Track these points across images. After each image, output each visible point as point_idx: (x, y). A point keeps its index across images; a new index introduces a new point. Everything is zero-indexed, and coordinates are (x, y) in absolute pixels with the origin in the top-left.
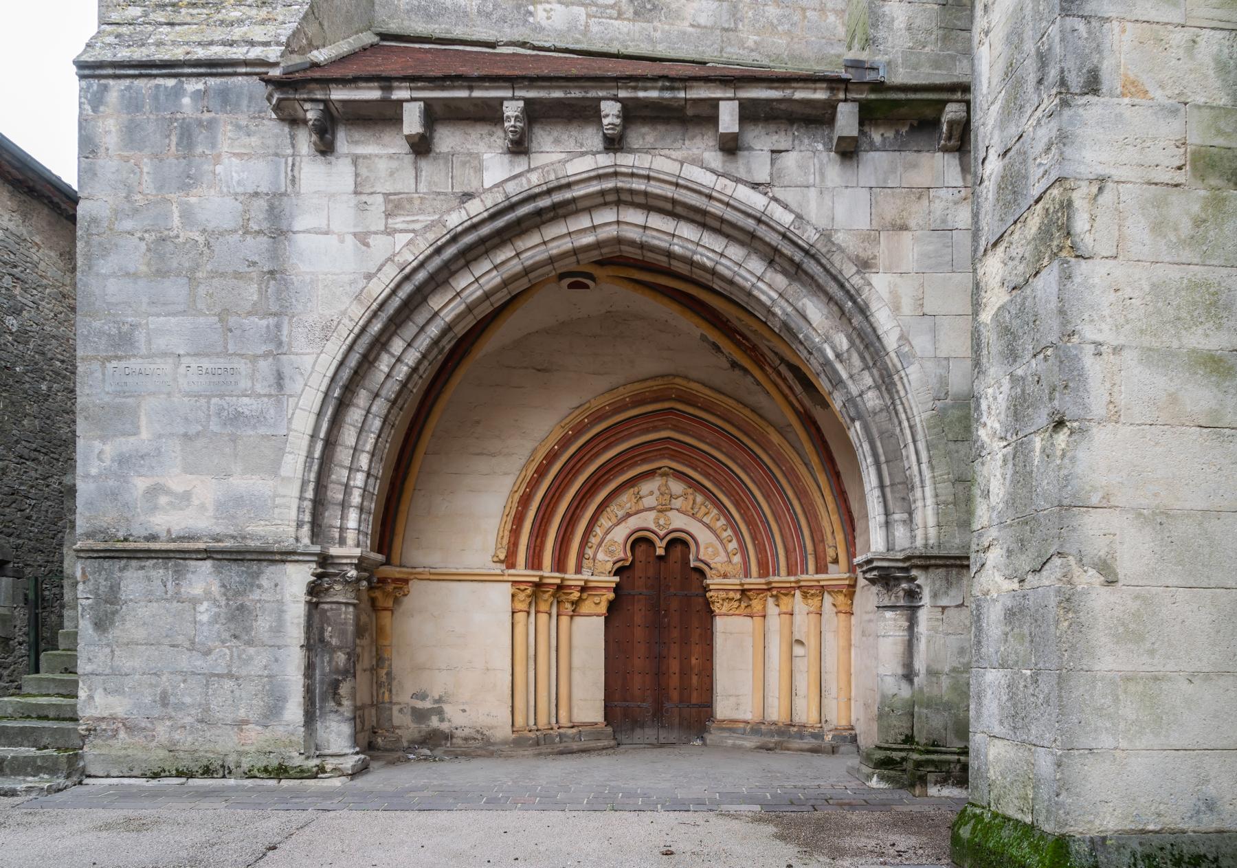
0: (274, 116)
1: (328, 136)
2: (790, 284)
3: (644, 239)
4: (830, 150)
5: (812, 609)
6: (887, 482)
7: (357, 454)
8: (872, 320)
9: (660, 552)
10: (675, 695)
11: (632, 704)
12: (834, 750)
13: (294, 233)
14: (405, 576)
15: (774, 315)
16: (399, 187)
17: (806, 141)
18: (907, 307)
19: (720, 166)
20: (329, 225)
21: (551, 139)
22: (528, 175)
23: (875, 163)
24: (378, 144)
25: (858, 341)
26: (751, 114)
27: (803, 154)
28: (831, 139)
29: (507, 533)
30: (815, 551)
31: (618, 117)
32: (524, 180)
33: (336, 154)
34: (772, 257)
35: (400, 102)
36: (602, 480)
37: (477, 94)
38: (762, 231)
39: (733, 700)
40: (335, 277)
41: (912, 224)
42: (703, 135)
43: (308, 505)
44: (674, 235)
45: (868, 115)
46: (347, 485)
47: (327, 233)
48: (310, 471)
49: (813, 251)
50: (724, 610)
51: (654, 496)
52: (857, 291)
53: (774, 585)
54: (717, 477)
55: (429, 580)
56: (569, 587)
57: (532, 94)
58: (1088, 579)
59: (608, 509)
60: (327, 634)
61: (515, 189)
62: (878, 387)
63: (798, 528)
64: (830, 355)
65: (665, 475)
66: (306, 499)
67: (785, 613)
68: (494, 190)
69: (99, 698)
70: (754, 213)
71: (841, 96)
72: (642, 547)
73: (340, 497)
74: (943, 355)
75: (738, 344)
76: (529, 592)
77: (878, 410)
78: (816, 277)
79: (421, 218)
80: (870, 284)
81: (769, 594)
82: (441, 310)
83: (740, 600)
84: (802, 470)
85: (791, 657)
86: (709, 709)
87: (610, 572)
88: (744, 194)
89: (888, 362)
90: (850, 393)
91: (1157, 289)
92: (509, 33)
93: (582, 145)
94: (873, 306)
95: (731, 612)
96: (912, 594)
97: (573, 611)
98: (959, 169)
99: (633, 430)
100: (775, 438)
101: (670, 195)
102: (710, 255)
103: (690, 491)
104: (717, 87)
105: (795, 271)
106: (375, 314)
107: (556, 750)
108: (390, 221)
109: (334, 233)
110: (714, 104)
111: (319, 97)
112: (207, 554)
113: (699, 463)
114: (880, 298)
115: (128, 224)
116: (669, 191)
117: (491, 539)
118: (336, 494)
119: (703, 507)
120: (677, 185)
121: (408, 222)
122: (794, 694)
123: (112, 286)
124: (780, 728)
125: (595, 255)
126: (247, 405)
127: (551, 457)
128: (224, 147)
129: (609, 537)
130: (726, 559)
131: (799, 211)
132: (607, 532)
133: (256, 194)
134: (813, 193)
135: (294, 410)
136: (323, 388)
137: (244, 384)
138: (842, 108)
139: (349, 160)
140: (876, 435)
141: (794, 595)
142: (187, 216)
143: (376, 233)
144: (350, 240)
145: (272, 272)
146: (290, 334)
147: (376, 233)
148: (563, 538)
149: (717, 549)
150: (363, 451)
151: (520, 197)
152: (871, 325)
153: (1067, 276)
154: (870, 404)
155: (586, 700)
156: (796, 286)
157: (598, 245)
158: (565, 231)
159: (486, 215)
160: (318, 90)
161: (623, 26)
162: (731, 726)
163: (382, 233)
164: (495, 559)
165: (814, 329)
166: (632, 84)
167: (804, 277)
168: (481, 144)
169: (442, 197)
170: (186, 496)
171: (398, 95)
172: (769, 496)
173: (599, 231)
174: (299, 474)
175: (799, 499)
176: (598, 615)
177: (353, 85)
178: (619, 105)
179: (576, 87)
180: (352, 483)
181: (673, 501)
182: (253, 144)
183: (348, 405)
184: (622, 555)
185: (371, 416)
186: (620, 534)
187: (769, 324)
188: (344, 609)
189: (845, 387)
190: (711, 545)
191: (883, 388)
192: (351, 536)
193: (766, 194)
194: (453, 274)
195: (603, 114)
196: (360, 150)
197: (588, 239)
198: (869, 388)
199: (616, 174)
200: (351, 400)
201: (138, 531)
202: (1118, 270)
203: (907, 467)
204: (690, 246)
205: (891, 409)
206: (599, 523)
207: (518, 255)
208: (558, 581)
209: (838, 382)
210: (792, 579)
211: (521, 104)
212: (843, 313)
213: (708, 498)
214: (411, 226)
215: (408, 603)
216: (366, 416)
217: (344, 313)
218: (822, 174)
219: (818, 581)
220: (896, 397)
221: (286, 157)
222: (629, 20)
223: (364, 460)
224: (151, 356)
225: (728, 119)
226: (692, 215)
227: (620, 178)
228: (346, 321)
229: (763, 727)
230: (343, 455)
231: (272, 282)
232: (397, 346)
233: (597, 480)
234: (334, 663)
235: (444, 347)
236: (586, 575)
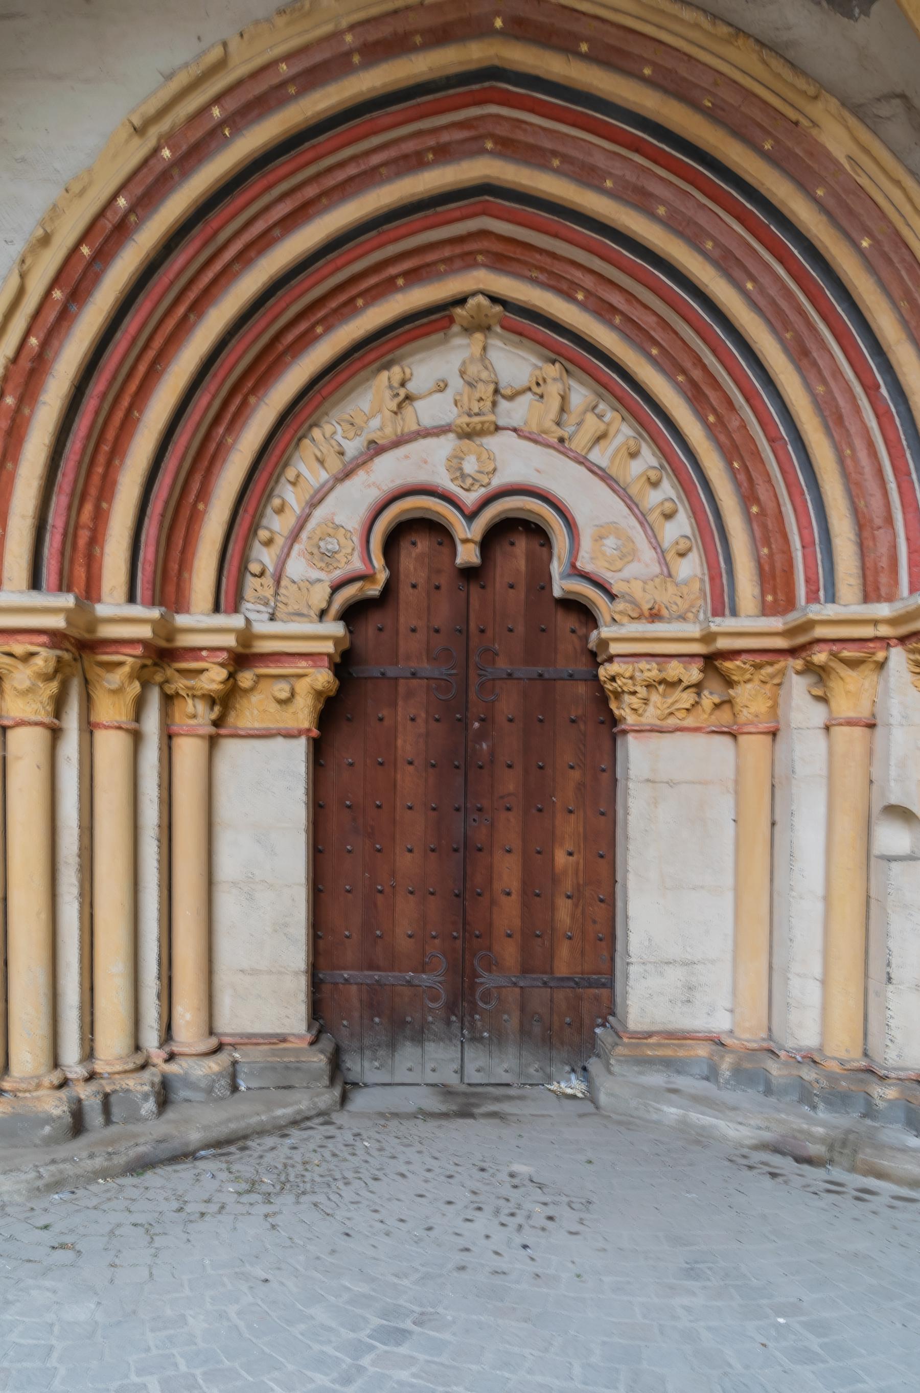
9: (467, 555)
10: (509, 953)
11: (389, 977)
36: (290, 337)
39: (675, 975)
51: (449, 394)
53: (820, 632)
54: (636, 314)
56: (194, 652)
59: (316, 433)
67: (850, 723)
81: (799, 664)
83: (698, 687)
86: (604, 992)
95: (672, 722)
97: (217, 723)
99: (376, 159)
103: (553, 371)
107: (120, 1160)
113: (578, 275)
119: (590, 418)
124: (832, 1077)
129: (319, 514)
130: (656, 569)
132: (315, 502)
141: (881, 666)
149: (630, 540)
155: (254, 972)
172: (805, 353)
176: (289, 735)
181: (503, 404)
184: (357, 565)
206: (290, 473)
210: (883, 610)
229: (774, 1069)
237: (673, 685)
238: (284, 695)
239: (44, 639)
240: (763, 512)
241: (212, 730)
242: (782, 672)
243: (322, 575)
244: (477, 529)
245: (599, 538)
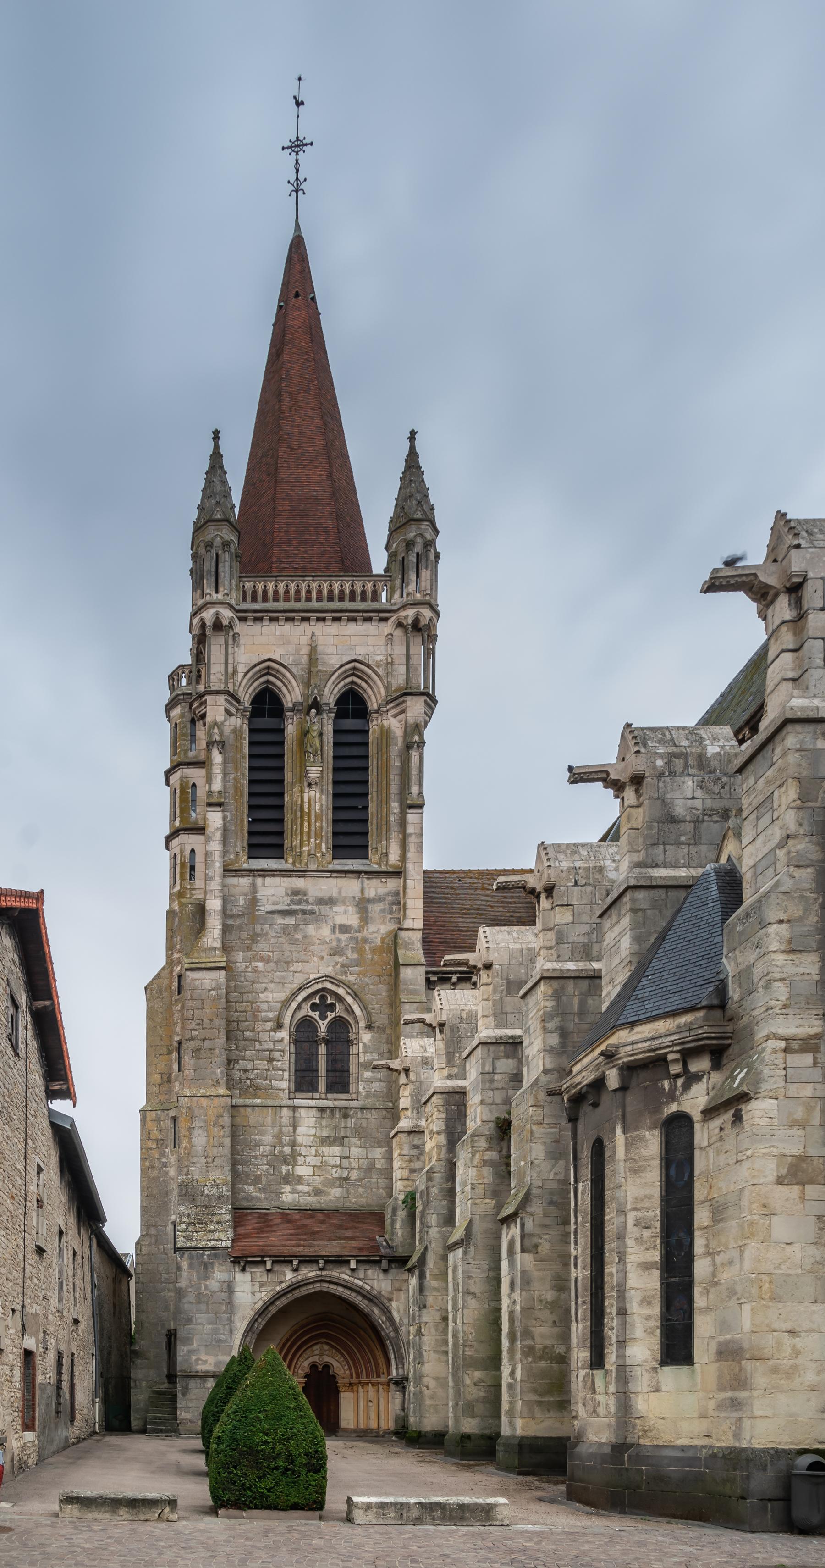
9: (320, 1369)
12: (383, 1436)
18: (402, 1311)
23: (393, 1272)
26: (358, 1262)
34: (364, 1297)
45: (390, 1262)
58: (425, 1388)
63: (369, 1359)
69: (183, 1414)
84: (371, 1343)
88: (357, 1281)
91: (437, 1340)
92: (274, 1204)
100: (362, 1333)
105: (370, 1300)
112: (213, 1376)
115: (190, 1290)
123: (186, 1306)
126: (222, 1337)
128: (216, 1269)
137: (222, 1332)
142: (206, 1287)
153: (420, 1339)
161: (311, 1199)
162: (346, 1430)
170: (206, 1361)
186: (306, 1364)
196: (253, 1270)
197: (313, 1291)
201: (193, 1370)
202: (429, 1337)
209: (383, 1329)
224: (197, 1324)
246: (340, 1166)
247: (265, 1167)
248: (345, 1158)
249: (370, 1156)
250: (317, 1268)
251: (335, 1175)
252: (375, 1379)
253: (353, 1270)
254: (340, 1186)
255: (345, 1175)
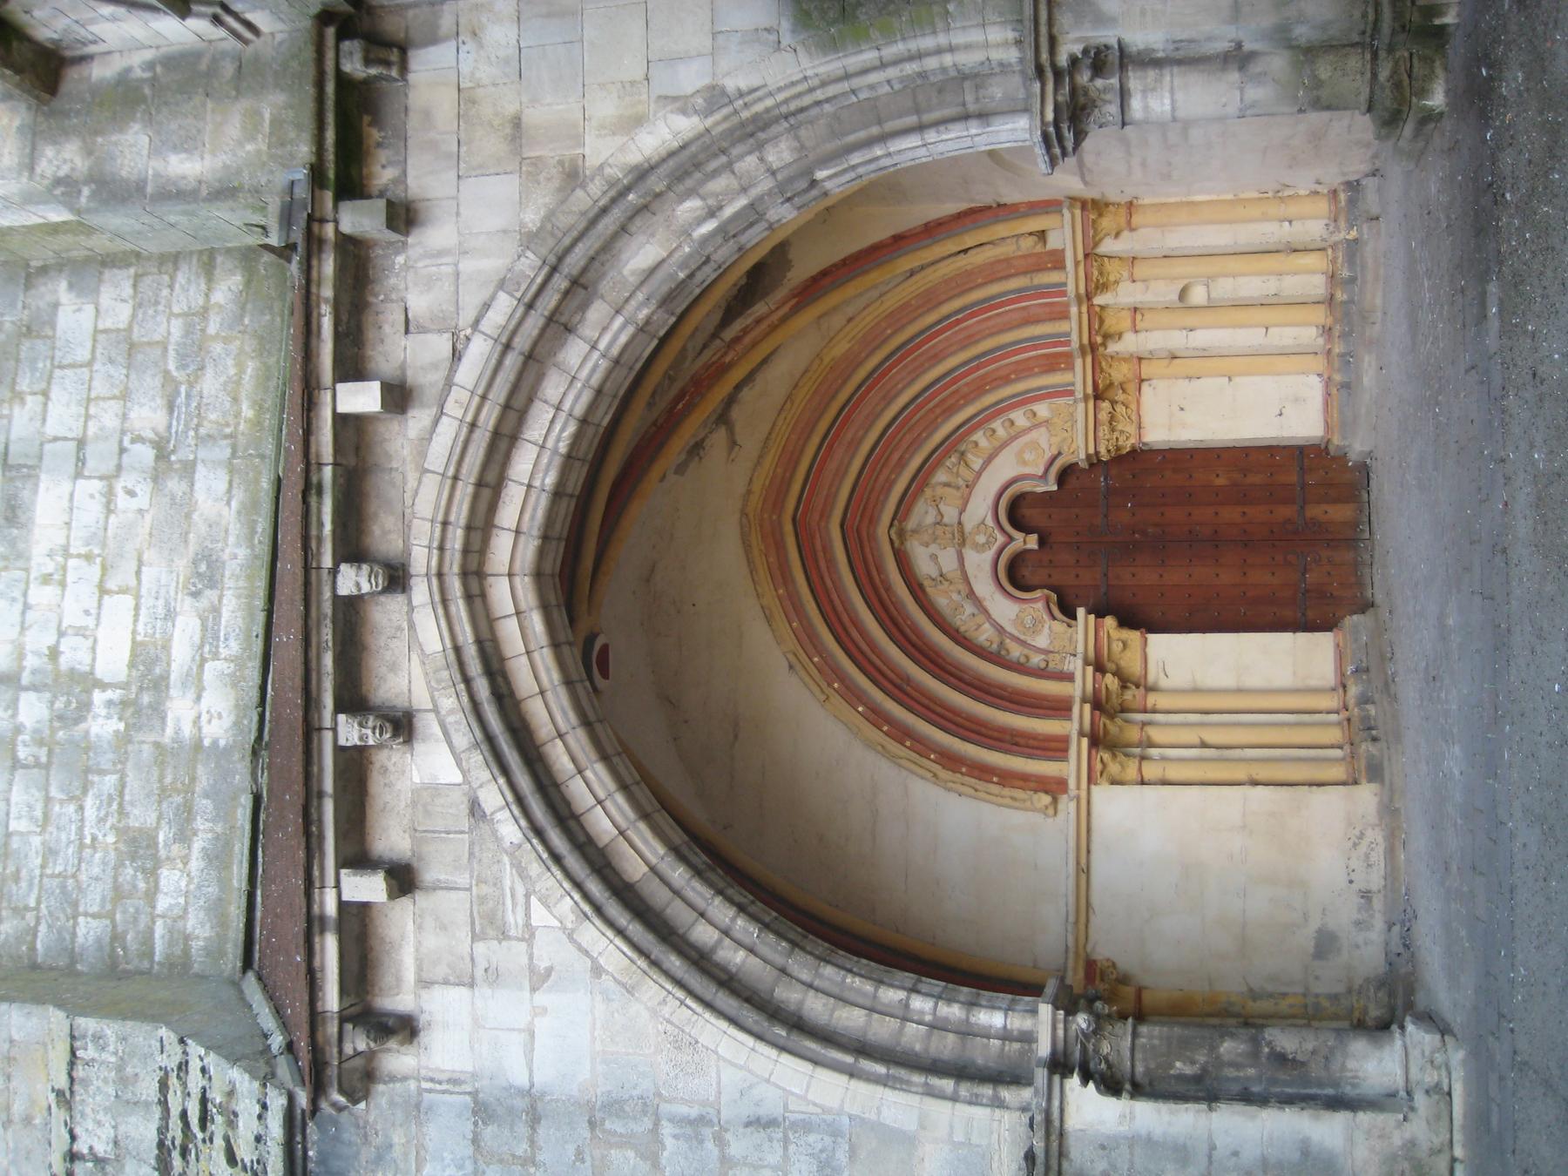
0: (362, 1105)
1: (391, 1022)
2: (602, 297)
3: (535, 532)
4: (405, 244)
5: (1126, 274)
6: (911, 120)
7: (879, 1008)
8: (656, 158)
9: (1032, 542)
13: (532, 1085)
14: (1081, 964)
15: (648, 322)
16: (462, 917)
17: (393, 281)
19: (428, 411)
20: (520, 1030)
21: (390, 676)
22: (443, 712)
24: (400, 946)
25: (689, 183)
26: (352, 368)
27: (410, 285)
28: (390, 244)
29: (1007, 791)
30: (1025, 273)
31: (359, 568)
32: (450, 719)
33: (416, 1012)
34: (559, 326)
35: (342, 905)
36: (914, 638)
37: (328, 785)
38: (522, 343)
40: (598, 1025)
41: (511, 109)
42: (385, 440)
43: (965, 1089)
44: (529, 486)
45: (351, 187)
46: (932, 1026)
47: (532, 1035)
48: (908, 1082)
49: (552, 259)
50: (1131, 429)
52: (611, 185)
53: (1085, 341)
54: (904, 445)
55: (1087, 927)
57: (328, 701)
60: (1189, 1070)
61: (464, 736)
62: (760, 146)
64: (709, 226)
65: (902, 534)
66: (956, 1092)
68: (466, 768)
70: (496, 355)
71: (329, 229)
72: (1026, 573)
73: (951, 1037)
74: (708, 43)
75: (690, 408)
76: (1106, 756)
77: (796, 144)
78: (591, 252)
79: (507, 883)
80: (601, 167)
82: (647, 862)
83: (1113, 403)
85: (1210, 306)
87: (1069, 626)
89: (720, 129)
90: (770, 190)
93: (399, 628)
94: (634, 157)
96: (1098, 60)
97: (1138, 687)
98: (432, 49)
101: (470, 489)
102: (558, 427)
103: (928, 492)
104: (318, 416)
105: (581, 287)
106: (655, 964)
108: (513, 933)
109: (531, 1023)
110: (341, 420)
111: (336, 1030)
114: (622, 149)
116: (465, 490)
117: (1018, 818)
118: (946, 1046)
120: (456, 478)
121: (514, 905)
122: (1274, 300)
124: (1336, 321)
125: (560, 617)
127: (877, 717)
130: (1043, 430)
131: (493, 285)
133: (476, 1141)
134: (467, 266)
135: (809, 1102)
136: (773, 1053)
138: (346, 227)
139: (424, 994)
140: (838, 143)
141: (1102, 308)
143: (531, 957)
144: (541, 998)
145: (592, 1124)
146: (684, 1101)
147: (531, 957)
148: (1011, 702)
150: (875, 997)
151: (475, 725)
152: (664, 160)
154: (788, 157)
156: (604, 286)
157: (545, 608)
158: (524, 660)
159: (502, 781)
160: (325, 1030)
163: (531, 946)
164: (1051, 811)
165: (670, 255)
166: (314, 545)
167: (591, 275)
168: (399, 786)
169: (477, 849)
171: (331, 908)
172: (935, 356)
173: (523, 606)
174: (914, 1100)
175: (941, 303)
177: (318, 975)
178: (344, 567)
179: (319, 633)
180: (928, 1018)
181: (946, 520)
182: (403, 1141)
183: (800, 1018)
184: (1040, 605)
185: (817, 983)
186: (1004, 608)
187: (662, 333)
188: (1143, 1040)
189: (761, 198)
190: (1020, 454)
191: (762, 136)
192: (1018, 1022)
193: (468, 339)
194: (590, 840)
195: (355, 592)
196: (409, 975)
197: (537, 622)
198: (762, 159)
199: (440, 575)
200: (794, 1014)
203: (887, 88)
204: (545, 460)
205: (790, 117)
207: (561, 736)
208: (1087, 707)
209: (754, 212)
210: (1074, 310)
211: (342, 718)
212: (645, 207)
213: (939, 463)
214: (521, 899)
215: (1126, 961)
216: (817, 990)
217: (654, 1013)
218: (440, 253)
219: (1077, 263)
220: (777, 112)
221: (420, 1091)
222: (221, 597)
223: (891, 996)
225: (361, 398)
226: (498, 457)
227: (446, 569)
228: (666, 1011)
230: (882, 1030)
231: (608, 1125)
232: (703, 934)
233: (914, 646)
234: (1240, 1059)
235: (704, 863)
236: (1075, 665)
237: (1112, 418)
238: (1121, 645)
239: (1094, 752)
240: (1014, 372)
241: (1142, 689)
242: (1105, 356)
243: (1047, 626)
244: (1018, 536)
245: (1025, 463)
246: (109, 479)
247: (90, 813)
248: (81, 461)
249: (83, 354)
250: (395, 603)
251: (143, 500)
252: (1071, 279)
253: (398, 396)
254: (189, 469)
255: (146, 454)
